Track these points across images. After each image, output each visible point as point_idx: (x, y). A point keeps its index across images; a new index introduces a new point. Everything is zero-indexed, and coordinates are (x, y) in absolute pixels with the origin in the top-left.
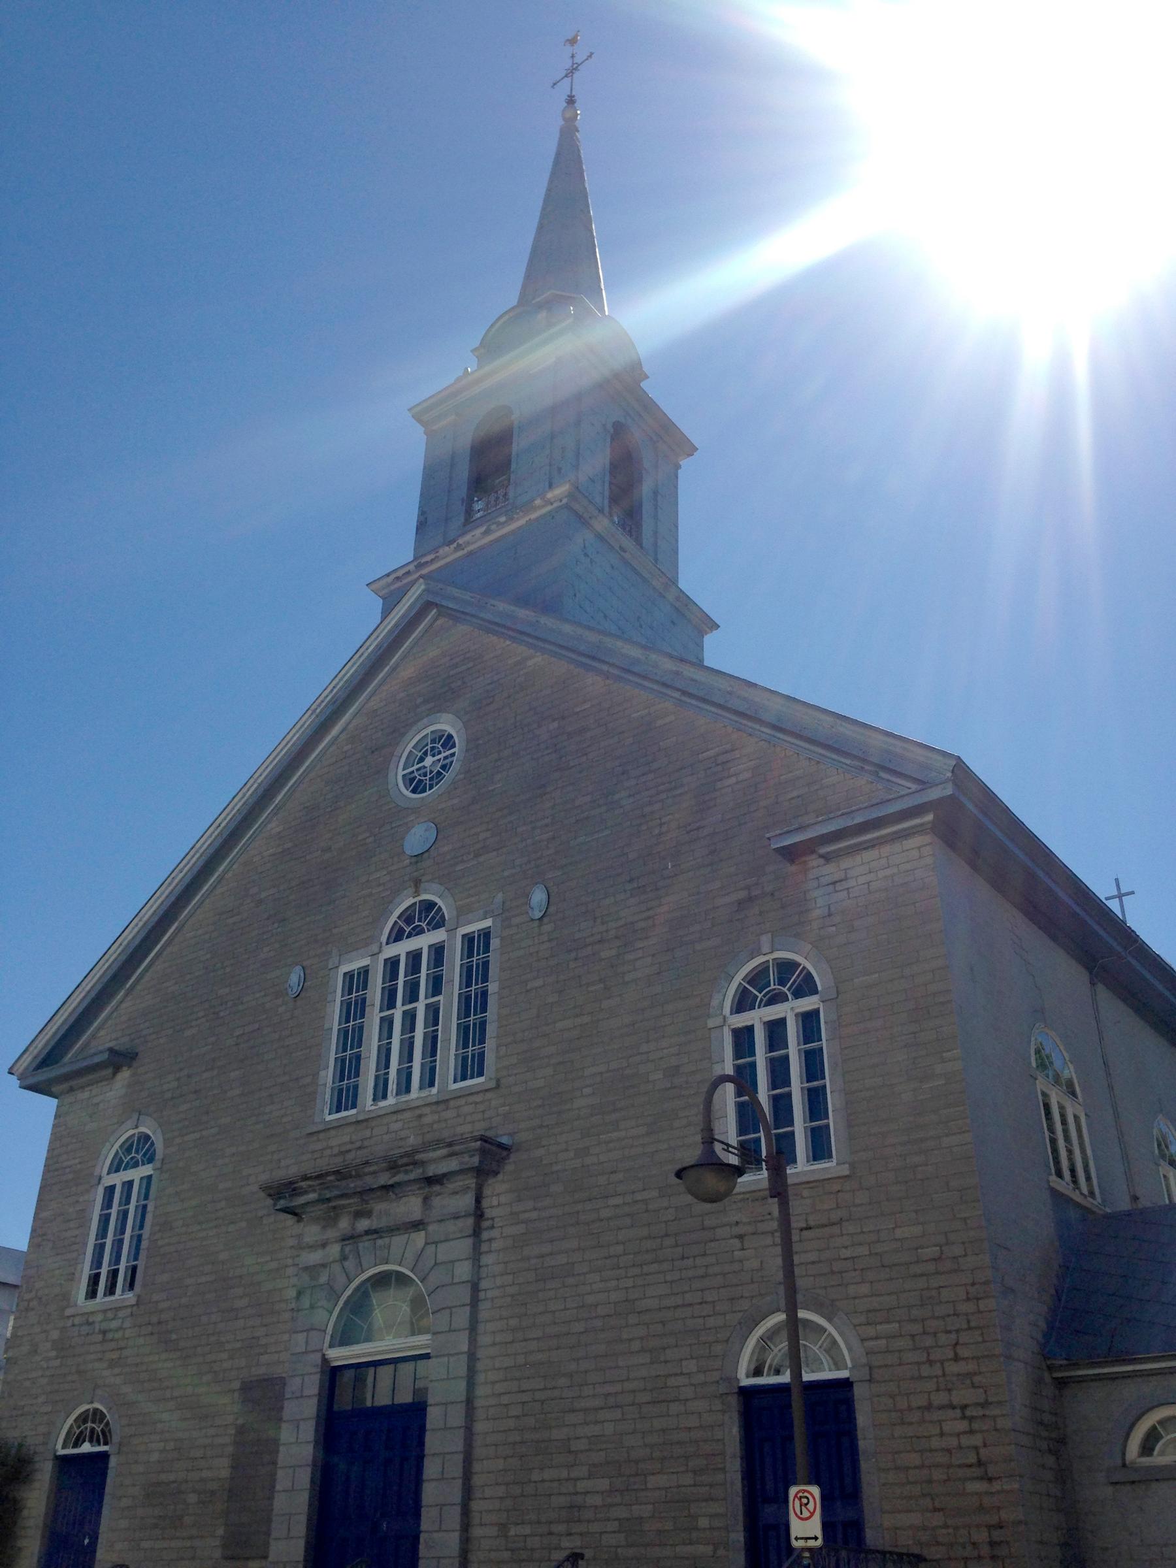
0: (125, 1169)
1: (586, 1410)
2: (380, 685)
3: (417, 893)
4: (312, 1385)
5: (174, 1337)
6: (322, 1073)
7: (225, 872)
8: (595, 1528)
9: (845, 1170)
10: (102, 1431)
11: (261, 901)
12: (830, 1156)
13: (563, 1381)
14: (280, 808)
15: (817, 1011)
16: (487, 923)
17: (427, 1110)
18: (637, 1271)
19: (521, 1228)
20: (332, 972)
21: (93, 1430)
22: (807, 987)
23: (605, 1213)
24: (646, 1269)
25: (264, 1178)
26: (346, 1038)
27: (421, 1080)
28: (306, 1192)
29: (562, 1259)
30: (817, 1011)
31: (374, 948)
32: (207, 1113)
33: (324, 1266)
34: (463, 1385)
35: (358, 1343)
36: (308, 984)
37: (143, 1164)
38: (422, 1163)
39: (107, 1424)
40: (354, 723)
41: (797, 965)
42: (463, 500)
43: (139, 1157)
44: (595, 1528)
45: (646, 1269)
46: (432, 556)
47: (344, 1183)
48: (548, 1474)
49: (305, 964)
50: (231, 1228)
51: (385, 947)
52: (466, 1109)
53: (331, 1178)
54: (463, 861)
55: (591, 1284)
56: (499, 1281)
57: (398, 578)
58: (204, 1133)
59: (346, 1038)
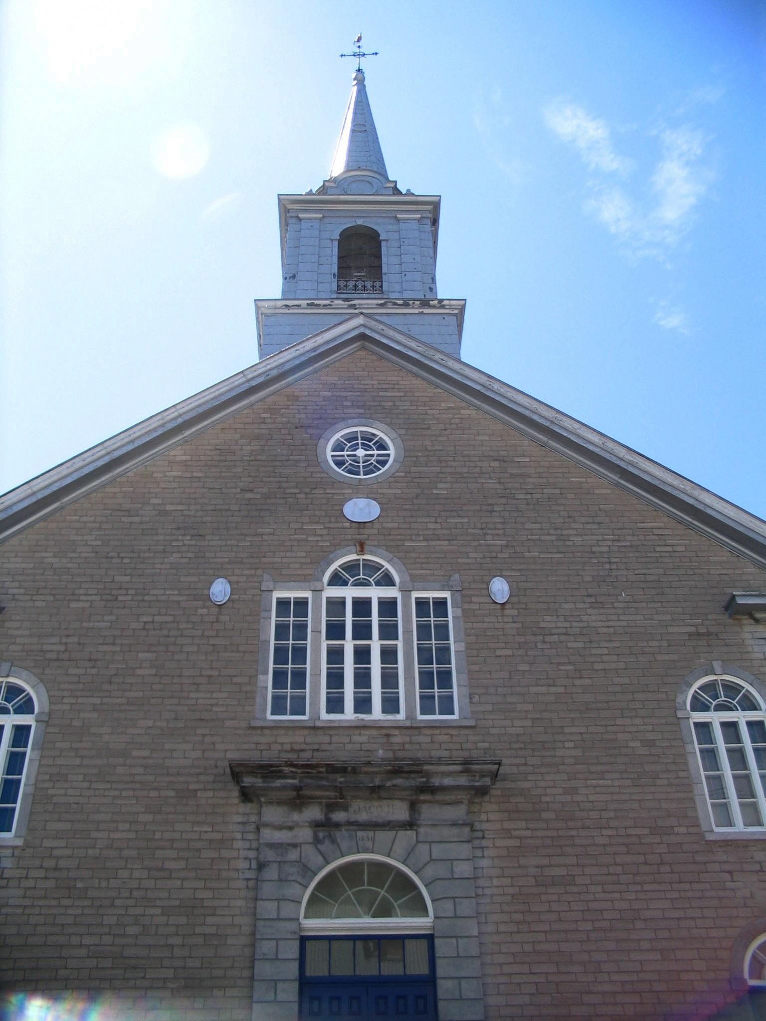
3: (362, 551)
4: (291, 950)
6: (261, 677)
7: (119, 476)
9: (19, 842)
11: (165, 513)
12: (10, 831)
15: (29, 727)
16: (446, 594)
17: (396, 732)
18: (638, 887)
20: (264, 595)
22: (26, 707)
23: (600, 840)
24: (646, 887)
25: (234, 755)
28: (285, 777)
29: (562, 871)
30: (29, 727)
31: (317, 585)
32: (110, 683)
33: (295, 846)
34: (295, 966)
35: (327, 917)
38: (428, 775)
40: (271, 399)
41: (23, 691)
42: (334, 275)
45: (646, 887)
46: (328, 302)
47: (331, 776)
50: (153, 794)
52: (442, 738)
53: (323, 769)
54: (411, 540)
55: (594, 893)
56: (495, 882)
57: (287, 306)
58: (105, 700)
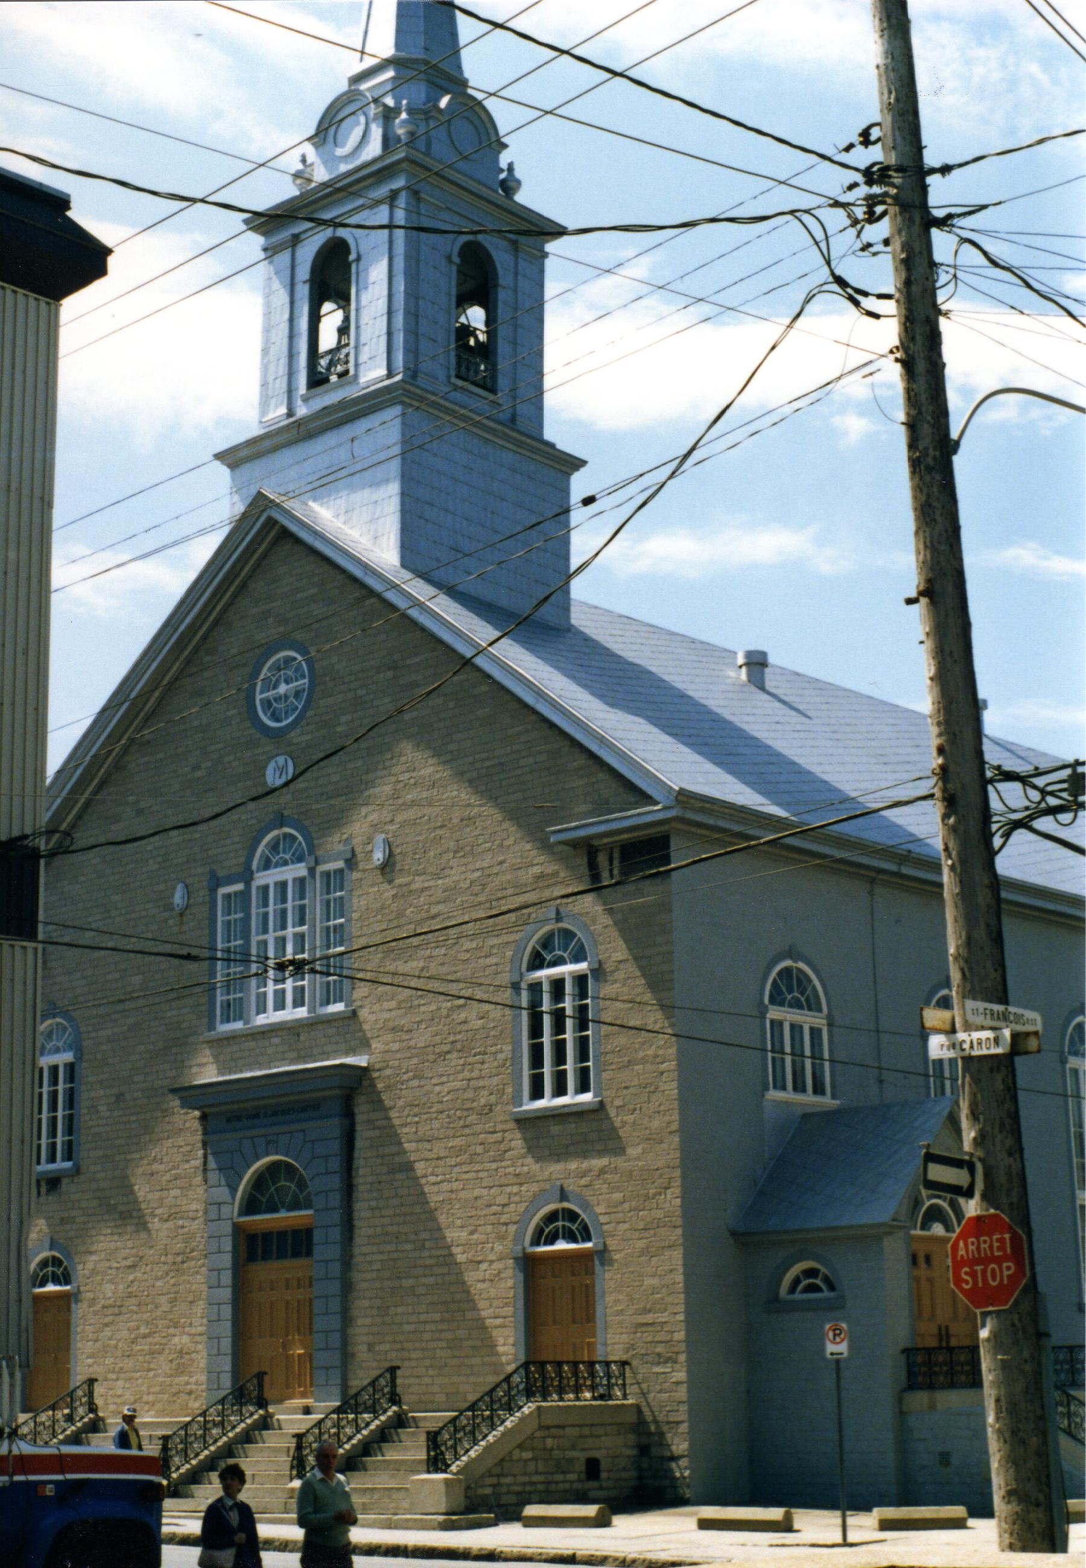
0: (49, 1053)
1: (425, 1267)
2: (243, 539)
5: (112, 1202)
8: (431, 1345)
10: (63, 1274)
13: (409, 1247)
14: (538, 694)
19: (377, 1133)
21: (53, 1272)
26: (229, 931)
27: (275, 924)
36: (192, 901)
37: (65, 1051)
39: (66, 1268)
43: (61, 1044)
44: (431, 1345)
48: (400, 1310)
49: (189, 881)
51: (256, 875)
59: (229, 931)
